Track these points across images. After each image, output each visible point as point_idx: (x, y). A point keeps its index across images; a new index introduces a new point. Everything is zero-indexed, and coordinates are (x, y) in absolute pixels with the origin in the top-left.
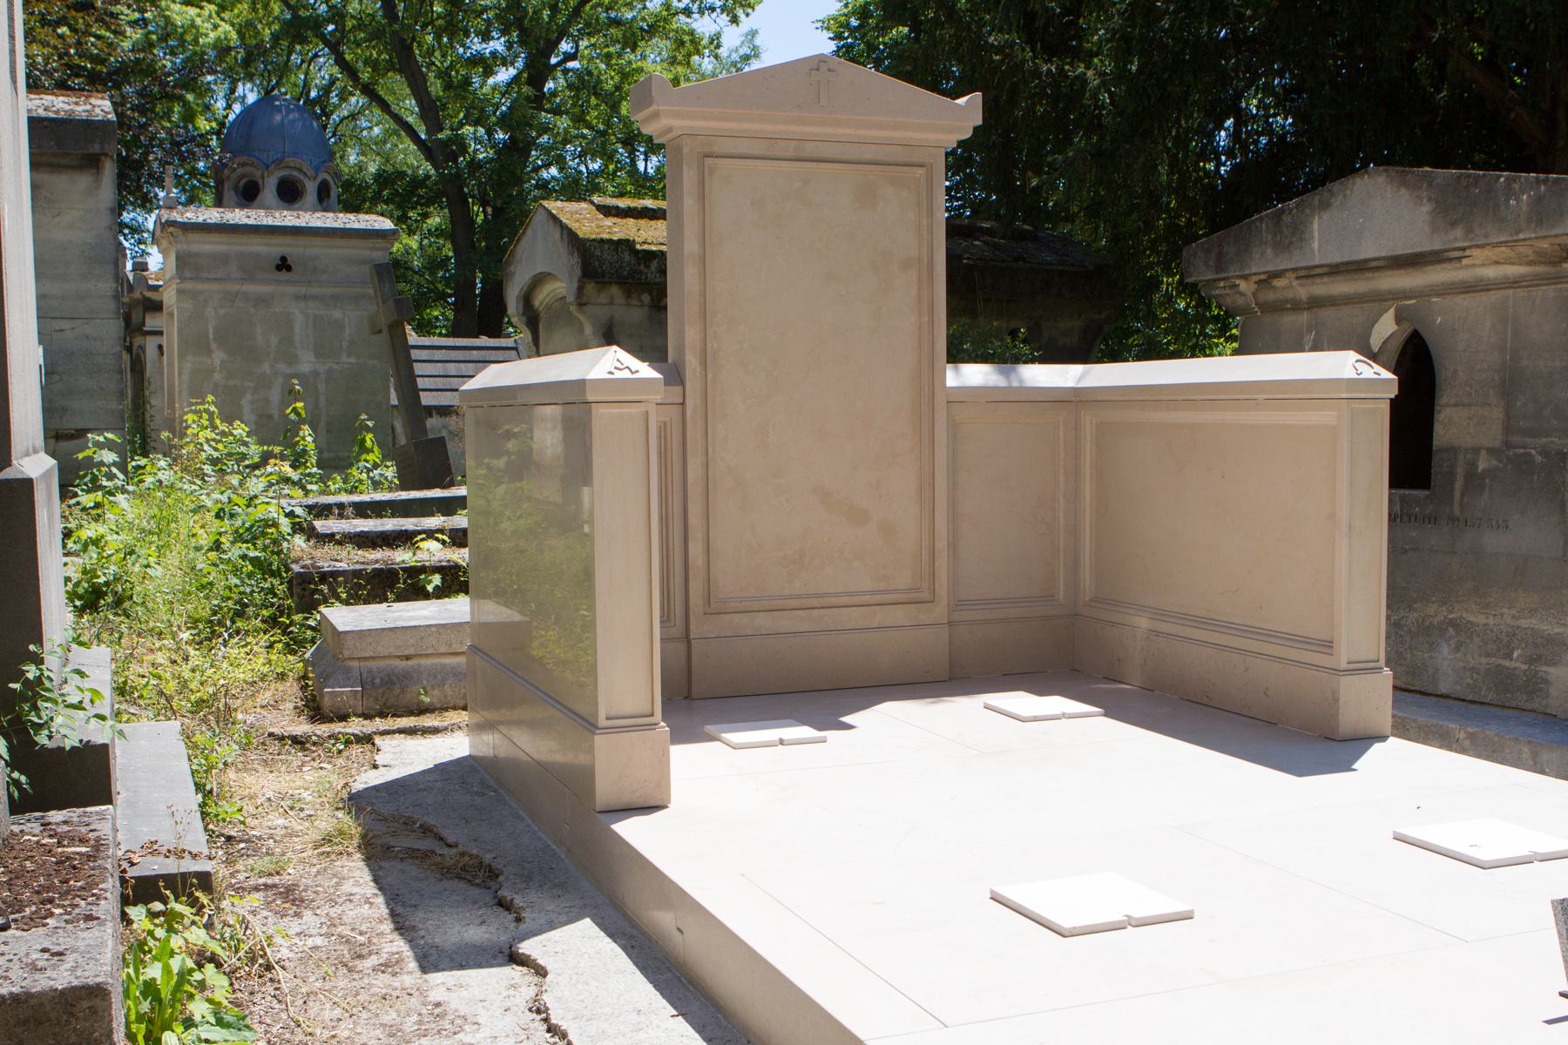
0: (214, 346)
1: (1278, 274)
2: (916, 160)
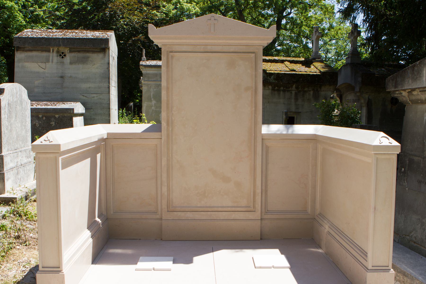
0: (152, 99)
1: (414, 90)
2: (252, 51)
